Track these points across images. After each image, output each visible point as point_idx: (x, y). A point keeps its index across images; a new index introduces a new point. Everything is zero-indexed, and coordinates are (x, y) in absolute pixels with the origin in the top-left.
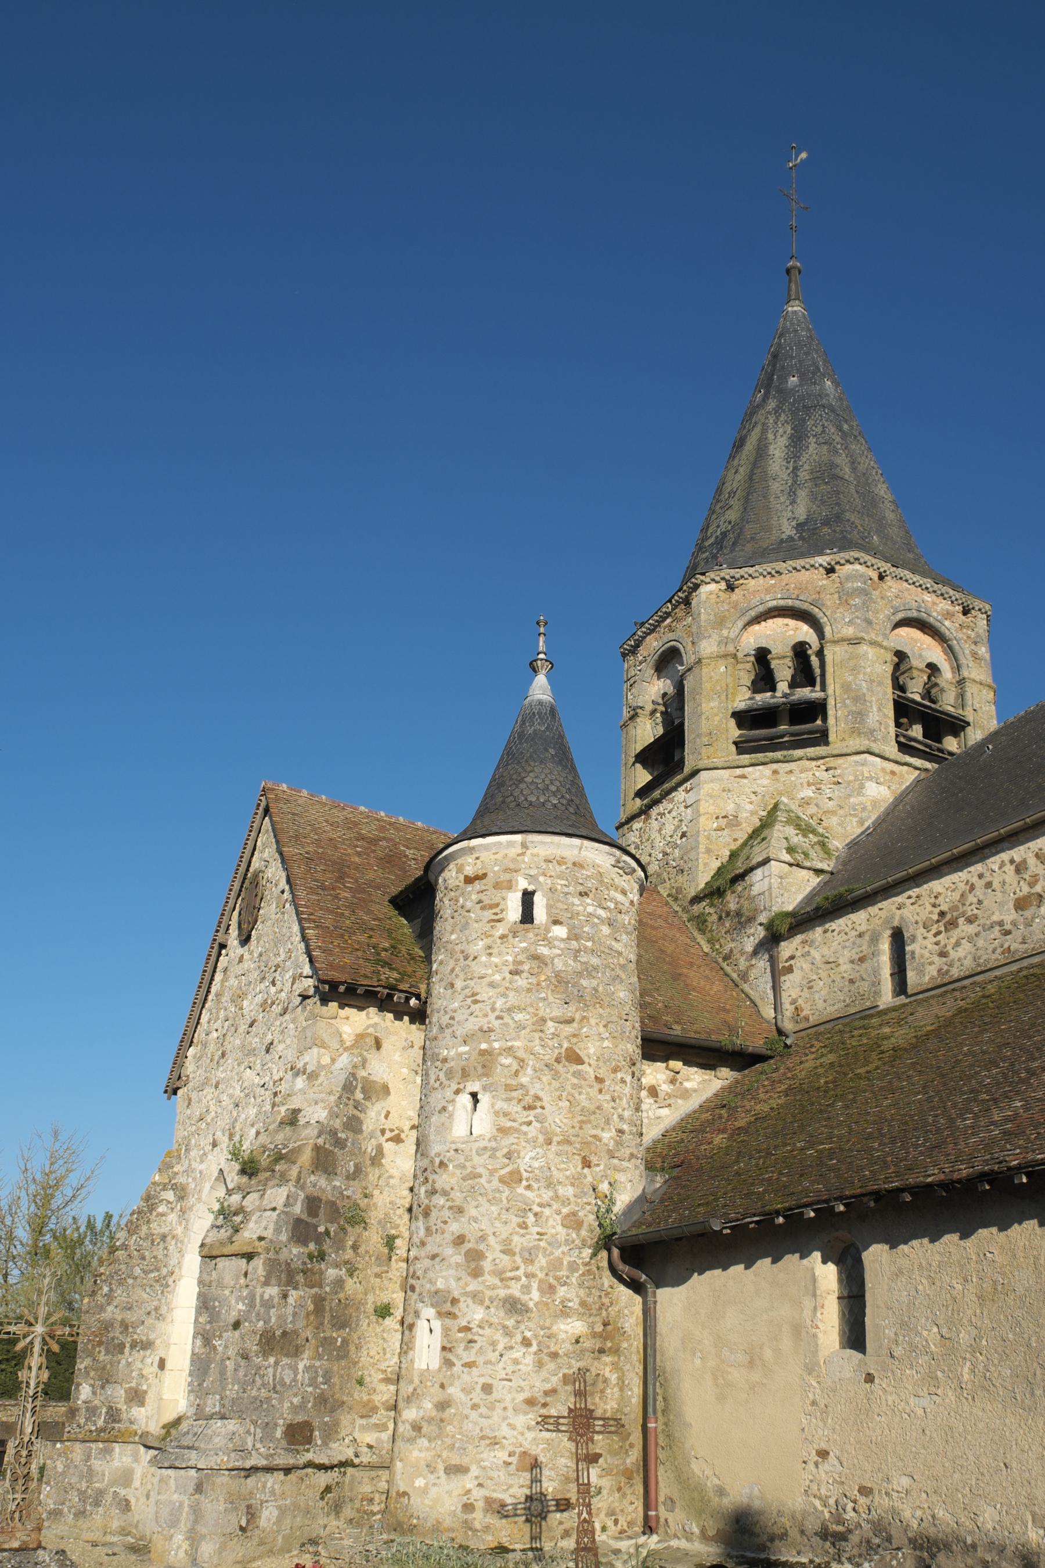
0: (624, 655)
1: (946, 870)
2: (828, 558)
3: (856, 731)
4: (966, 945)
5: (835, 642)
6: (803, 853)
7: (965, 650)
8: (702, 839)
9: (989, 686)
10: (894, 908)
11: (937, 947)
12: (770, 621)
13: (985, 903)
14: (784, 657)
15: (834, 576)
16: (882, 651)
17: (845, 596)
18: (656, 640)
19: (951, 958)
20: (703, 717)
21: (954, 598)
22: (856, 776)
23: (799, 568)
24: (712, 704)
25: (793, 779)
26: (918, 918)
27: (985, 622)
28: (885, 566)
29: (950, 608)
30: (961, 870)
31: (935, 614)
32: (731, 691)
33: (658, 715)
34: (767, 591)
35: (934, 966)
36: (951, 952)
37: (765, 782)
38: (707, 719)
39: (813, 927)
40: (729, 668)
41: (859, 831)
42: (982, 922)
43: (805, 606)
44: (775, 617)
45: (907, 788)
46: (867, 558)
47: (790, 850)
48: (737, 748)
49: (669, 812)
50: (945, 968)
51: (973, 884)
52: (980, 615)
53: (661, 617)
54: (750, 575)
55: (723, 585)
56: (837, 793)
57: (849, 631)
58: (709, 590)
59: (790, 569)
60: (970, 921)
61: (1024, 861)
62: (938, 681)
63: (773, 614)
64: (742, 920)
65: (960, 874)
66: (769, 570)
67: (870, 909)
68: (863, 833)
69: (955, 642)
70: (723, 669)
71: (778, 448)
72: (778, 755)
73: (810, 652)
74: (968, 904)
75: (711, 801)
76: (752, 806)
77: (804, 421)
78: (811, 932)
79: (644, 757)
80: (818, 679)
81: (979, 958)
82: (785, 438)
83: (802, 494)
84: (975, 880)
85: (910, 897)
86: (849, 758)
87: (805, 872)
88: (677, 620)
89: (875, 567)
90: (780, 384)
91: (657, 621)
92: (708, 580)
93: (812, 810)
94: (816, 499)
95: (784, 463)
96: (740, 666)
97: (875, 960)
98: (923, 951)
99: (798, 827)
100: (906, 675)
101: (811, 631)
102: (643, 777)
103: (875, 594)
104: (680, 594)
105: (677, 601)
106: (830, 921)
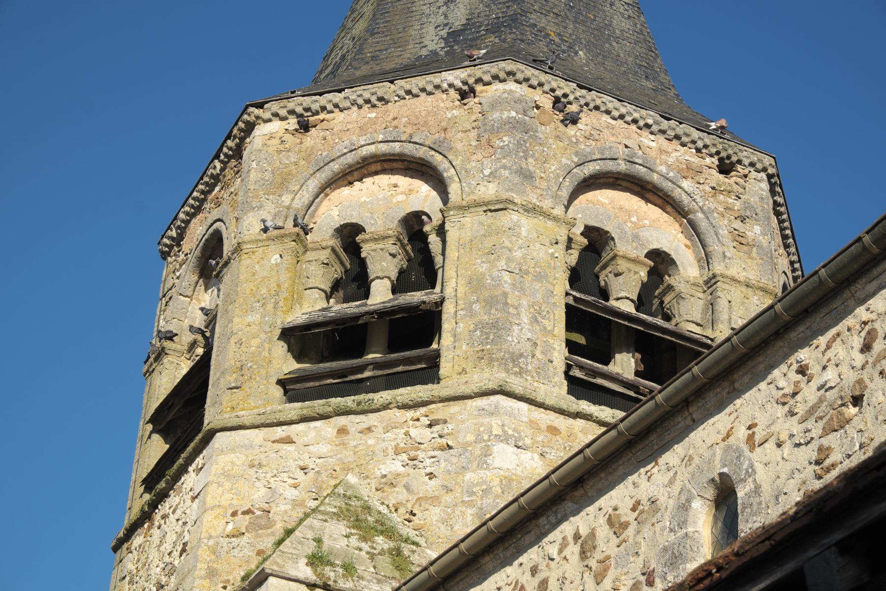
0: (165, 255)
2: (462, 74)
3: (483, 357)
5: (464, 208)
7: (720, 230)
8: (203, 553)
12: (368, 181)
14: (385, 238)
15: (471, 102)
16: (550, 223)
17: (486, 133)
20: (233, 341)
21: (700, 144)
22: (479, 435)
23: (415, 91)
24: (250, 319)
25: (371, 442)
29: (695, 160)
31: (663, 169)
34: (363, 130)
38: (240, 343)
43: (421, 152)
44: (376, 173)
46: (529, 72)
48: (286, 392)
52: (754, 174)
54: (336, 106)
56: (443, 464)
57: (489, 191)
58: (270, 133)
61: (592, 535)
63: (373, 168)
65: (508, 570)
66: (367, 95)
69: (700, 215)
72: (349, 401)
73: (427, 228)
75: (227, 485)
86: (469, 402)
89: (547, 88)
92: (267, 115)
93: (398, 495)
99: (357, 523)
100: (609, 269)
101: (434, 193)
105: (226, 155)
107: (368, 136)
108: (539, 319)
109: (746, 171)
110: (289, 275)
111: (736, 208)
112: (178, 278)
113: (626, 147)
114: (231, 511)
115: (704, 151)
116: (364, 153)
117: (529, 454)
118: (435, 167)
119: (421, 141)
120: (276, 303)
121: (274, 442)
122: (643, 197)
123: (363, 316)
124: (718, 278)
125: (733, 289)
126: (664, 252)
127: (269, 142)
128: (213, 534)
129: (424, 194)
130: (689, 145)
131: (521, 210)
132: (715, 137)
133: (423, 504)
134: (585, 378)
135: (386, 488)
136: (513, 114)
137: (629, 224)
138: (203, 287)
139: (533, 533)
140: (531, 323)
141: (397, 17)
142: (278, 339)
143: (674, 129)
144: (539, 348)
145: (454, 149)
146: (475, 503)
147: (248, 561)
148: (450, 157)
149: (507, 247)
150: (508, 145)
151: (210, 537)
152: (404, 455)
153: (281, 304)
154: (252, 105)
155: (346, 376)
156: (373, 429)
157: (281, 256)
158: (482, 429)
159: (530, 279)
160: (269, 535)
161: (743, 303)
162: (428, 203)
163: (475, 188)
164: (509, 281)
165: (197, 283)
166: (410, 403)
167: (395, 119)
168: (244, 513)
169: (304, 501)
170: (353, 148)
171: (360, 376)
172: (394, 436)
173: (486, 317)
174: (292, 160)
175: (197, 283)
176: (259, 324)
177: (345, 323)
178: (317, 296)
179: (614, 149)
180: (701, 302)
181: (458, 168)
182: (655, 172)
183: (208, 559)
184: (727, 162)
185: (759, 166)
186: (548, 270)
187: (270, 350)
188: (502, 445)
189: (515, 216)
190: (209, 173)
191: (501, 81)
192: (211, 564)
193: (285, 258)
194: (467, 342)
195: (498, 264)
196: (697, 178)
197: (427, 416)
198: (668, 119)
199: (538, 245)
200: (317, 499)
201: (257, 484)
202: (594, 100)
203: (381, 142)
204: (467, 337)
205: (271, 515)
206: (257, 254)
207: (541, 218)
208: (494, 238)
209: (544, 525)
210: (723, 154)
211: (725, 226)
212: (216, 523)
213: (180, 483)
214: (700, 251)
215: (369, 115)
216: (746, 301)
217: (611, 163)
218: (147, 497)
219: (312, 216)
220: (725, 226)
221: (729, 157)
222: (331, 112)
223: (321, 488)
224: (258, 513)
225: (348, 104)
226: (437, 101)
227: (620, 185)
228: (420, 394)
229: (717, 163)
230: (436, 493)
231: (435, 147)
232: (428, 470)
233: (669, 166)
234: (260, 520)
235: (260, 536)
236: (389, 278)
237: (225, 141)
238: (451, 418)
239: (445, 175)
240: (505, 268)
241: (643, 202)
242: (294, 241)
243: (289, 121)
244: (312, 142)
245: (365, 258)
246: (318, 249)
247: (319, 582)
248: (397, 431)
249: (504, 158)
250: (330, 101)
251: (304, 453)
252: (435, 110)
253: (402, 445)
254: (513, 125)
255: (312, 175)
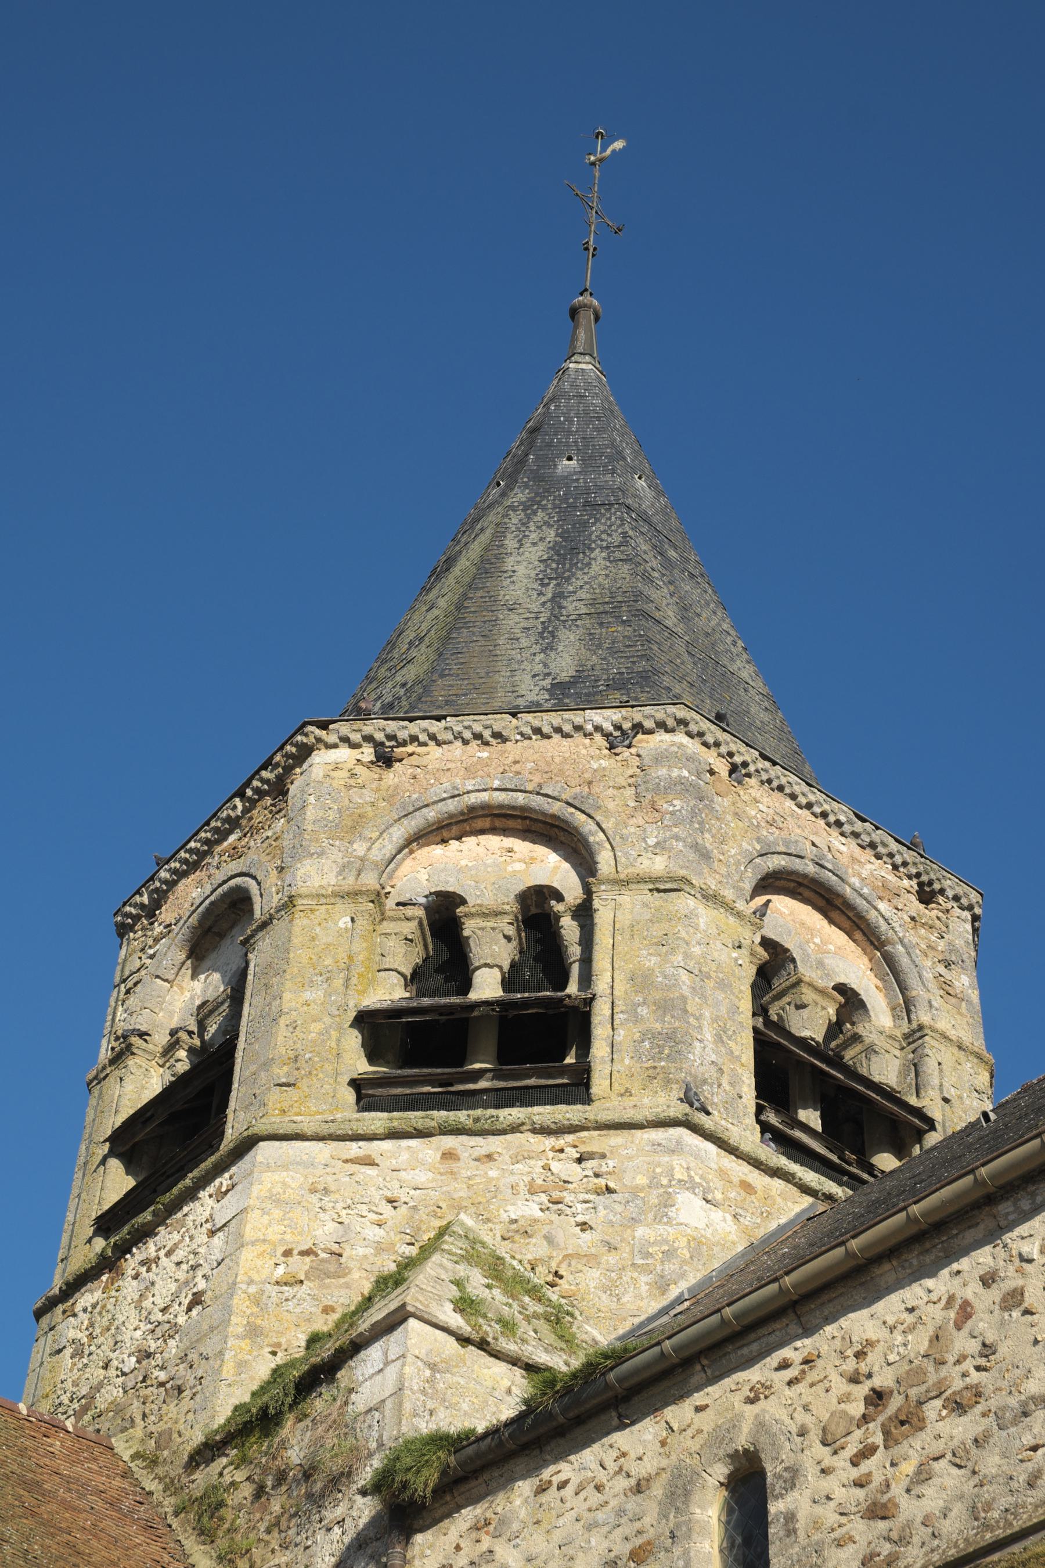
0: (123, 930)
1: (891, 1277)
4: (948, 1477)
5: (624, 883)
6: (499, 1321)
7: (924, 974)
8: (240, 1303)
9: (979, 1057)
10: (737, 1399)
11: (860, 1493)
12: (470, 841)
13: (1003, 1350)
14: (497, 914)
17: (647, 795)
18: (200, 883)
19: (901, 1519)
20: (283, 1021)
21: (898, 859)
23: (546, 729)
24: (308, 995)
25: (493, 1174)
26: (808, 1420)
27: (969, 927)
28: (745, 755)
29: (891, 877)
30: (932, 1274)
31: (855, 881)
32: (358, 969)
33: (182, 1054)
35: (851, 1548)
36: (905, 1502)
37: (422, 1177)
39: (507, 1482)
40: (359, 922)
41: (655, 1306)
42: (993, 1403)
44: (482, 832)
45: (782, 1228)
47: (465, 1305)
48: (359, 1099)
49: (168, 1254)
50: (886, 1548)
51: (966, 1304)
52: (957, 911)
53: (216, 830)
54: (433, 737)
55: (368, 753)
56: (602, 1212)
57: (658, 865)
58: (334, 765)
59: (528, 731)
60: (958, 1407)
62: (860, 1029)
63: (479, 824)
64: (317, 1484)
65: (929, 1283)
66: (478, 728)
67: (670, 1413)
68: (664, 1311)
70: (344, 922)
71: (524, 563)
72: (462, 1116)
74: (951, 1359)
75: (277, 1213)
76: (381, 1232)
77: (585, 525)
78: (500, 1498)
79: (127, 1143)
80: (575, 970)
81: (988, 1507)
82: (541, 546)
83: (569, 639)
84: (972, 1291)
85: (784, 1365)
86: (638, 1133)
87: (500, 1368)
88: (254, 831)
89: (723, 750)
90: (540, 467)
91: (206, 842)
92: (333, 738)
93: (535, 1249)
94: (599, 646)
95: (536, 586)
96: (388, 927)
97: (677, 1551)
98: (818, 1510)
100: (786, 999)
101: (567, 866)
102: (117, 1182)
103: (722, 803)
104: (264, 774)
106: (556, 1460)
107: (479, 780)
108: (725, 1038)
109: (949, 905)
110: (364, 945)
111: (940, 948)
112: (152, 957)
113: (813, 844)
114: (283, 1249)
115: (901, 869)
116: (474, 801)
117: (720, 1213)
118: (576, 829)
119: (555, 794)
120: (348, 979)
121: (346, 1161)
122: (826, 915)
123: (480, 1006)
124: (927, 1031)
125: (943, 1049)
126: (852, 989)
127: (332, 774)
128: (256, 1277)
129: (552, 865)
130: (885, 858)
131: (698, 895)
132: (915, 854)
133: (573, 1262)
134: (781, 1126)
135: (517, 1237)
136: (685, 773)
137: (812, 946)
138: (190, 972)
139: (982, 1226)
140: (715, 1042)
141: (476, 660)
142: (351, 1026)
143: (869, 834)
144: (725, 1076)
145: (604, 809)
146: (652, 1268)
147: (309, 1320)
148: (598, 818)
149: (684, 939)
150: (679, 811)
151: (251, 1282)
152: (543, 1195)
153: (354, 981)
154: (311, 723)
155: (451, 1085)
156: (496, 1156)
157: (353, 920)
158: (658, 1170)
159: (712, 985)
160: (341, 1286)
161: (955, 1069)
162: (558, 877)
163: (635, 860)
164: (688, 982)
165: (183, 964)
166: (553, 1126)
167: (516, 762)
168: (303, 1253)
169: (393, 1245)
170: (457, 792)
171: (471, 1086)
172: (527, 1169)
173: (658, 1026)
174: (368, 799)
175: (183, 964)
176: (322, 1004)
177: (452, 1014)
178: (395, 981)
179: (800, 844)
180: (897, 1062)
181: (610, 833)
182: (847, 883)
183: (248, 1312)
184: (927, 889)
185: (964, 901)
186: (732, 979)
187: (339, 1040)
188: (688, 1194)
189: (691, 902)
190: (224, 815)
191: (667, 731)
192: (252, 1319)
193: (358, 922)
194: (632, 1055)
195: (673, 958)
196: (894, 901)
197: (575, 1147)
198: (864, 820)
199: (719, 946)
200: (413, 1244)
201: (322, 1215)
202: (778, 778)
203: (496, 789)
204: (632, 1049)
205: (343, 1260)
206: (317, 913)
207: (722, 910)
208: (665, 926)
209: (1008, 1214)
210: (924, 878)
211: (930, 968)
212: (259, 1263)
213: (179, 1215)
214: (896, 996)
215: (479, 754)
216: (959, 1067)
217: (797, 860)
218: (99, 1243)
219: (390, 877)
220: (930, 968)
221: (930, 883)
222: (425, 744)
223: (419, 1229)
224: (323, 1255)
225: (449, 736)
226: (577, 746)
227: (800, 894)
228: (568, 1116)
229: (916, 887)
230: (593, 1250)
231: (576, 803)
232: (580, 1218)
233: (863, 879)
234: (327, 1265)
235: (328, 1287)
236: (500, 968)
237: (257, 772)
238: (612, 1152)
239: (591, 839)
240: (682, 964)
241: (825, 922)
242: (372, 902)
243: (364, 749)
244: (396, 780)
245: (468, 938)
246: (400, 919)
247: (475, 1336)
248: (532, 1162)
249: (676, 826)
250: (425, 730)
251: (392, 1179)
252: (575, 756)
253: (540, 1182)
254: (683, 787)
255: (396, 821)
